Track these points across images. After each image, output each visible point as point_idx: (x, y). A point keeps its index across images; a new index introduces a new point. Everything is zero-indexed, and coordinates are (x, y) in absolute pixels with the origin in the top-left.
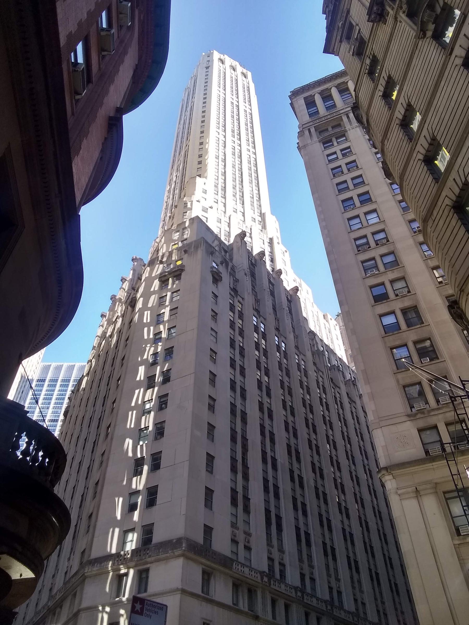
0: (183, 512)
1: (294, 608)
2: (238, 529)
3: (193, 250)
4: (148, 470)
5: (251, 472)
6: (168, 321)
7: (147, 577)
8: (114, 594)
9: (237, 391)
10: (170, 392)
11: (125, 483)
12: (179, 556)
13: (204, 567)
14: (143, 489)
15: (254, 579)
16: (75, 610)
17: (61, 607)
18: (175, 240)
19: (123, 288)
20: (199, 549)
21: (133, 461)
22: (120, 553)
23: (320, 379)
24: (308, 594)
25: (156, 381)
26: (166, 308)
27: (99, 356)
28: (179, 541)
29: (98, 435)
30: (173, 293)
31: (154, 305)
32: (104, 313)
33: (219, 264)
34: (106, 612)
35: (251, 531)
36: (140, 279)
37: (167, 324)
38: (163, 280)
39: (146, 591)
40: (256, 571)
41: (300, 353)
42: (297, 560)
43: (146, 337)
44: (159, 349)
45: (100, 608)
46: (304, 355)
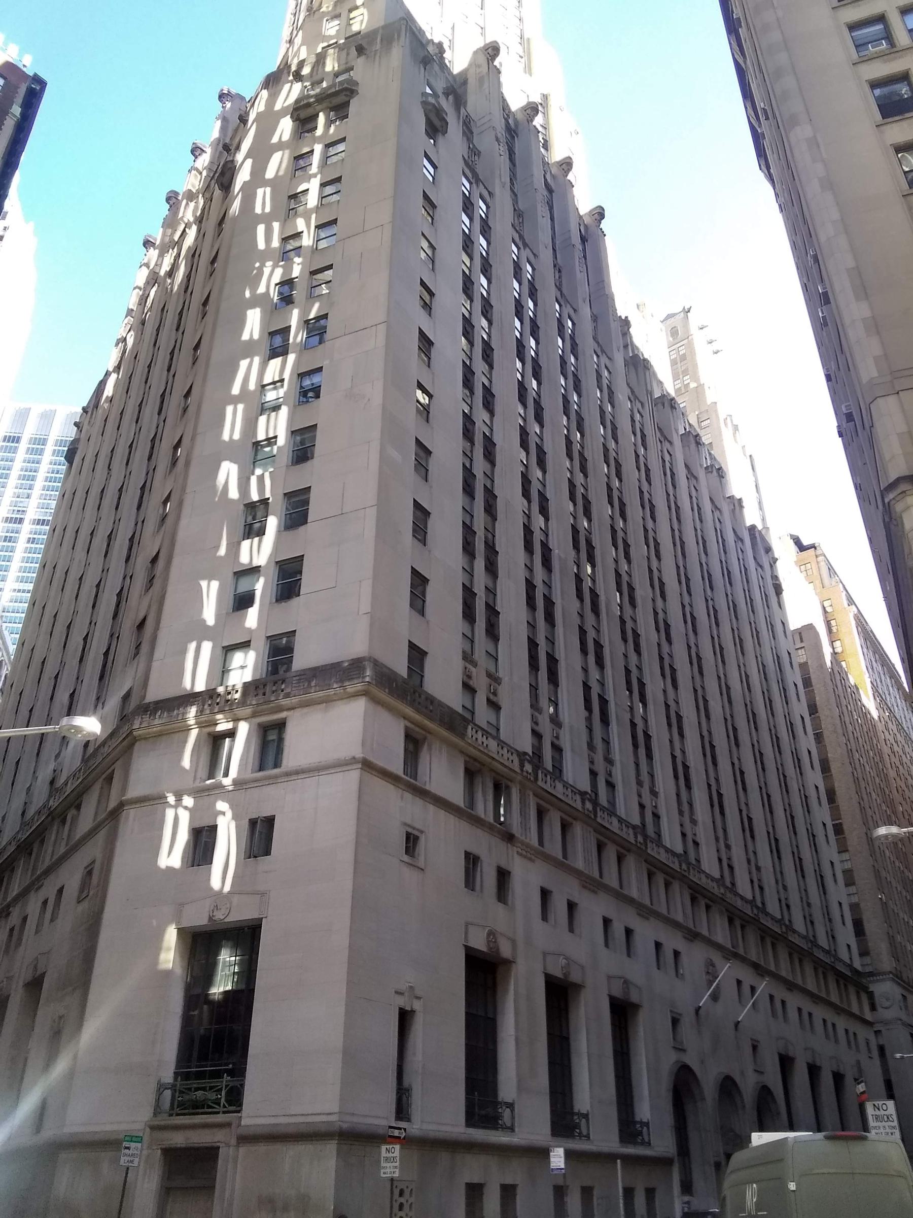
0: (366, 606)
1: (578, 830)
2: (475, 665)
3: (378, 46)
4: (279, 526)
5: (501, 560)
6: (317, 209)
7: (281, 740)
8: (203, 771)
9: (476, 392)
10: (325, 363)
11: (222, 551)
12: (356, 695)
13: (409, 724)
14: (268, 563)
15: (506, 763)
16: (112, 804)
17: (78, 807)
18: (331, 37)
19: (197, 170)
20: (399, 686)
21: (242, 507)
22: (215, 689)
23: (637, 417)
24: (603, 809)
25: (291, 340)
26: (312, 180)
27: (143, 324)
28: (357, 665)
29: (140, 524)
30: (328, 146)
31: (281, 173)
32: (150, 236)
33: (440, 94)
34: (186, 808)
35: (501, 674)
36: (243, 119)
37: (314, 216)
38: (304, 118)
39: (277, 764)
40: (512, 750)
41: (603, 351)
42: (585, 746)
43: (261, 245)
44: (296, 271)
45: (171, 799)
46: (610, 359)
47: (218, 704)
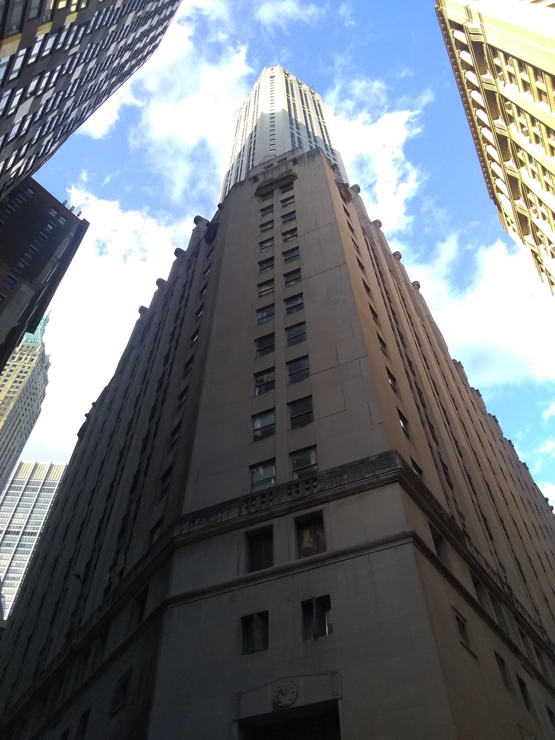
10: (304, 291)
16: (149, 610)
47: (253, 506)
